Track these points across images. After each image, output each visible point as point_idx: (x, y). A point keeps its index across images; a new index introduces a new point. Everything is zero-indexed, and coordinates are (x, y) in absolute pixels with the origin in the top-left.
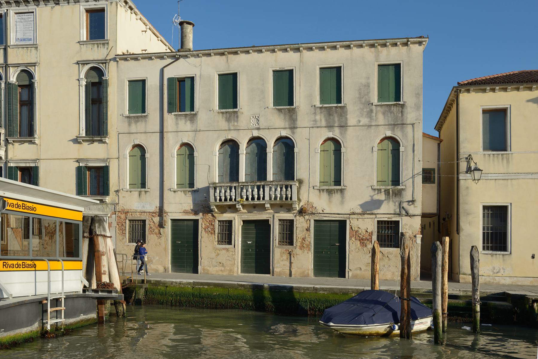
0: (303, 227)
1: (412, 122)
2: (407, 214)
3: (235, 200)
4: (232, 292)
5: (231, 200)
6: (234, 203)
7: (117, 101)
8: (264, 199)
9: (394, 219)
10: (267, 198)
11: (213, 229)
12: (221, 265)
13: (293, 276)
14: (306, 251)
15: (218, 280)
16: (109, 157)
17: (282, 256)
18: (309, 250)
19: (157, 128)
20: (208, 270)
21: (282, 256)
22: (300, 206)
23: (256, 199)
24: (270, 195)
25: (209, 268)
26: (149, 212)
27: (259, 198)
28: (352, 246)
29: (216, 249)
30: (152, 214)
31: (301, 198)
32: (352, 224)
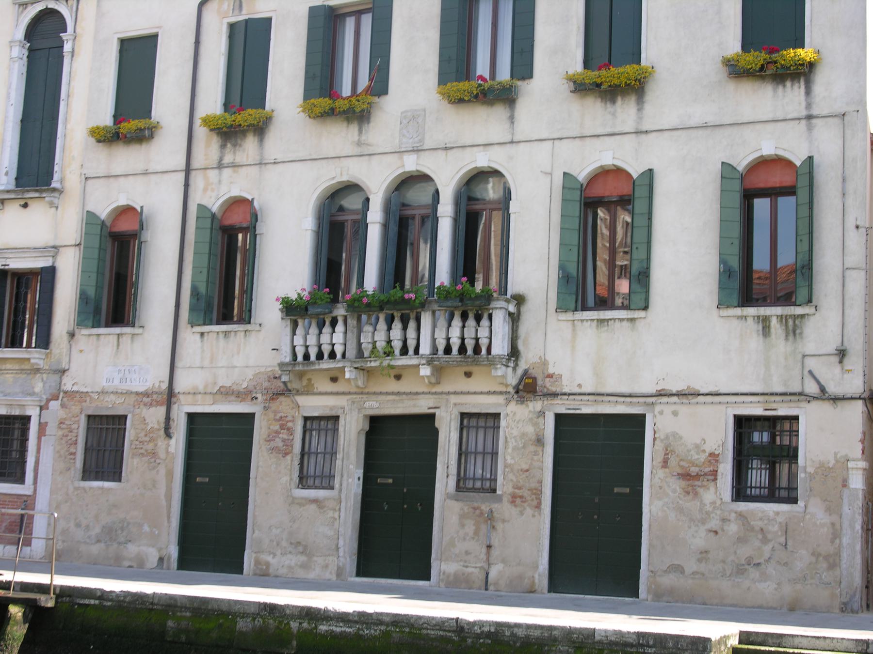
0: (523, 435)
1: (839, 108)
2: (374, 347)
3: (344, 356)
4: (521, 633)
5: (332, 355)
6: (340, 365)
7: (88, 91)
8: (417, 351)
9: (782, 412)
10: (425, 349)
11: (288, 444)
12: (301, 549)
13: (491, 588)
14: (529, 511)
15: (599, 600)
16: (58, 243)
17: (463, 526)
18: (538, 506)
19: (180, 161)
20: (268, 564)
21: (463, 526)
22: (520, 372)
23: (397, 352)
24: (434, 340)
25: (269, 558)
26: (137, 393)
27: (404, 351)
28: (659, 499)
29: (294, 501)
30: (146, 397)
31: (521, 346)
32: (660, 425)
